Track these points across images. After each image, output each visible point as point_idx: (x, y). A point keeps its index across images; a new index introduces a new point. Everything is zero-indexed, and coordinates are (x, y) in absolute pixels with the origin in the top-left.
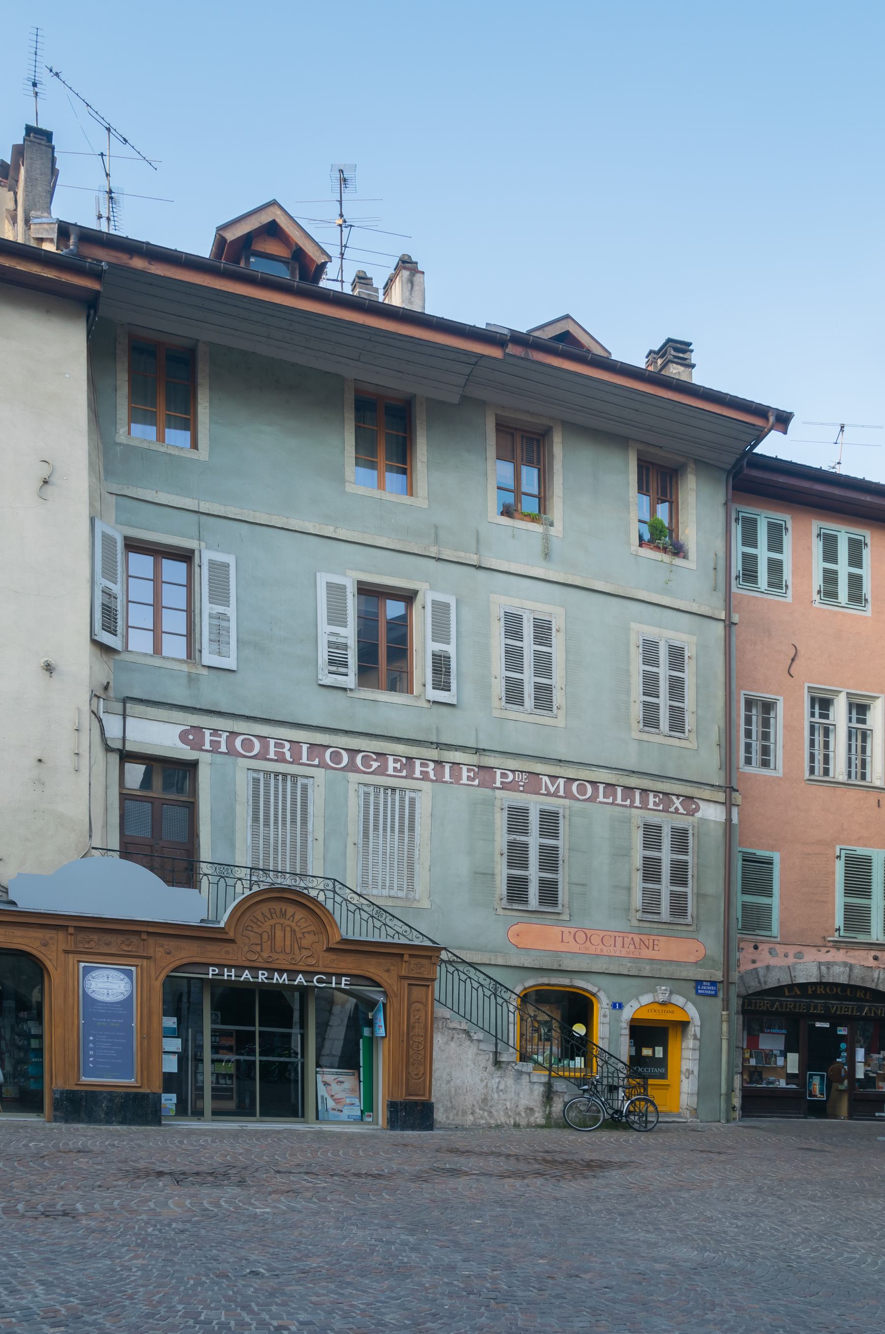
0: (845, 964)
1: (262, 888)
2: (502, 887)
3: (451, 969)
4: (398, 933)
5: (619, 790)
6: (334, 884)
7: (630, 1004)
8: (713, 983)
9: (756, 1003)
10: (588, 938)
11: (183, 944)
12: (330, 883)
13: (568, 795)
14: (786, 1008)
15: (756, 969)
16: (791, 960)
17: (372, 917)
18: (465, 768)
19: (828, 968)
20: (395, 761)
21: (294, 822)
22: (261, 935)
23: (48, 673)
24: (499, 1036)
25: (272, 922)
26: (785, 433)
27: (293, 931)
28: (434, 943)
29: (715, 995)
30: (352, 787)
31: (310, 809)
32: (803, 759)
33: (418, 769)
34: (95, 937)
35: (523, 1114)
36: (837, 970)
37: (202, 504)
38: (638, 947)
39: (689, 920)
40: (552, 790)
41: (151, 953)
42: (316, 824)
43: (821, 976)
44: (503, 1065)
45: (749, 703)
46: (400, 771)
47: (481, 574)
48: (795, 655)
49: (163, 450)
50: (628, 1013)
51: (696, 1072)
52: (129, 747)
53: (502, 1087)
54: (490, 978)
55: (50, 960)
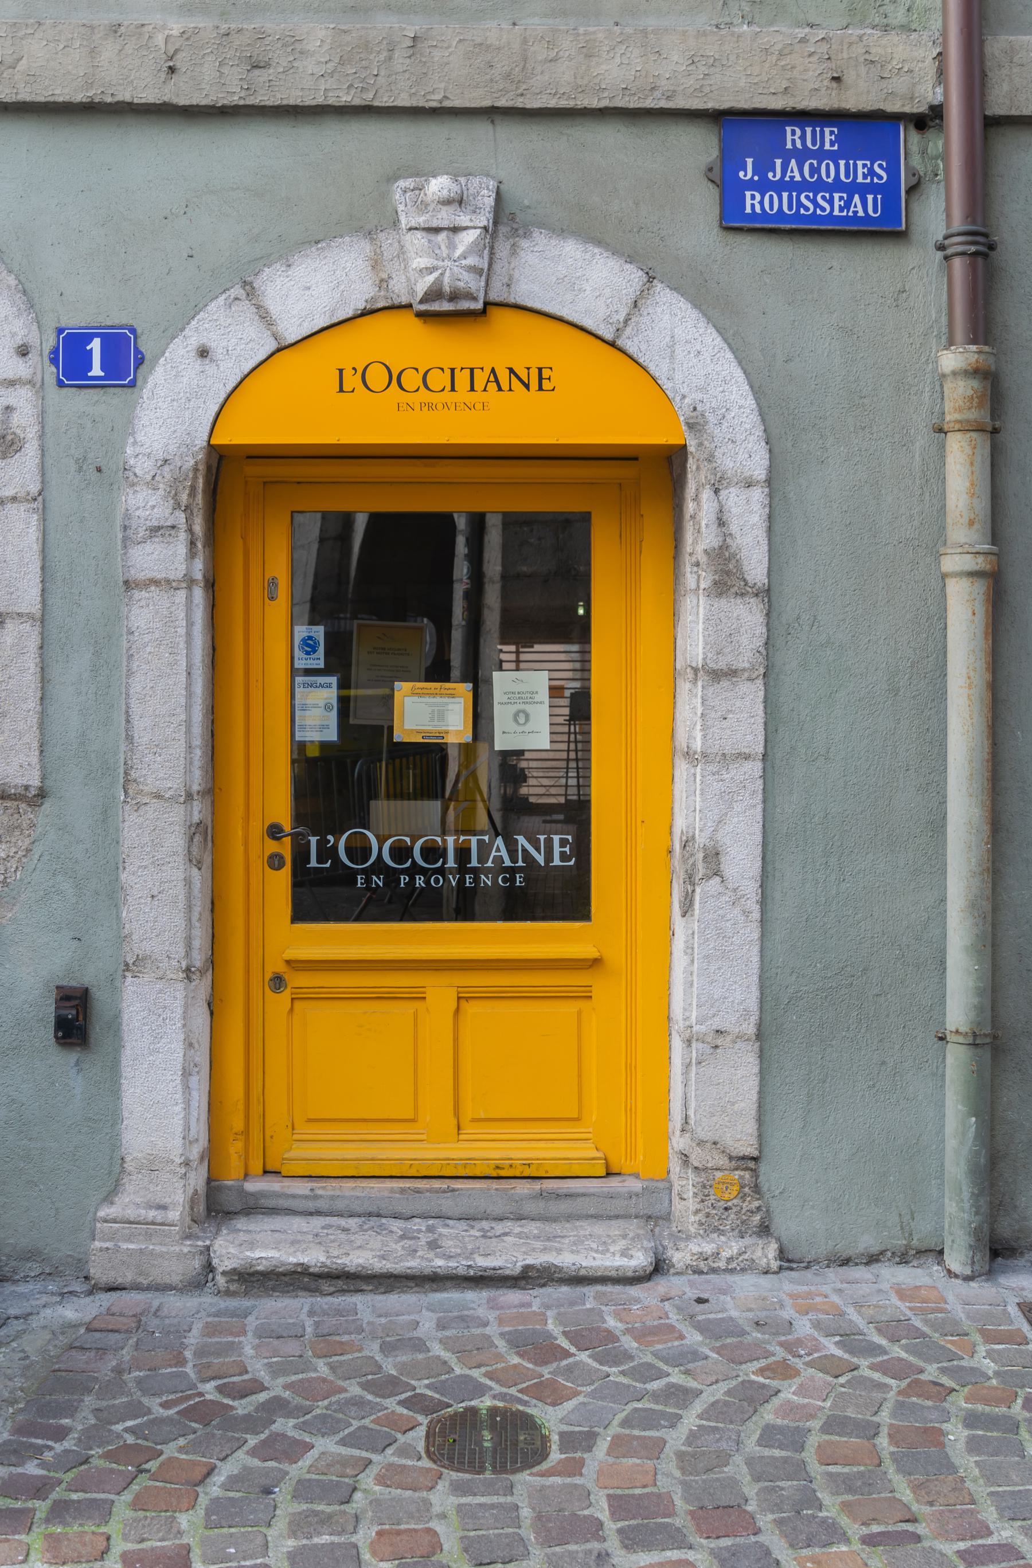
7: (192, 338)
8: (868, 129)
29: (887, 230)
50: (171, 415)
51: (742, 862)
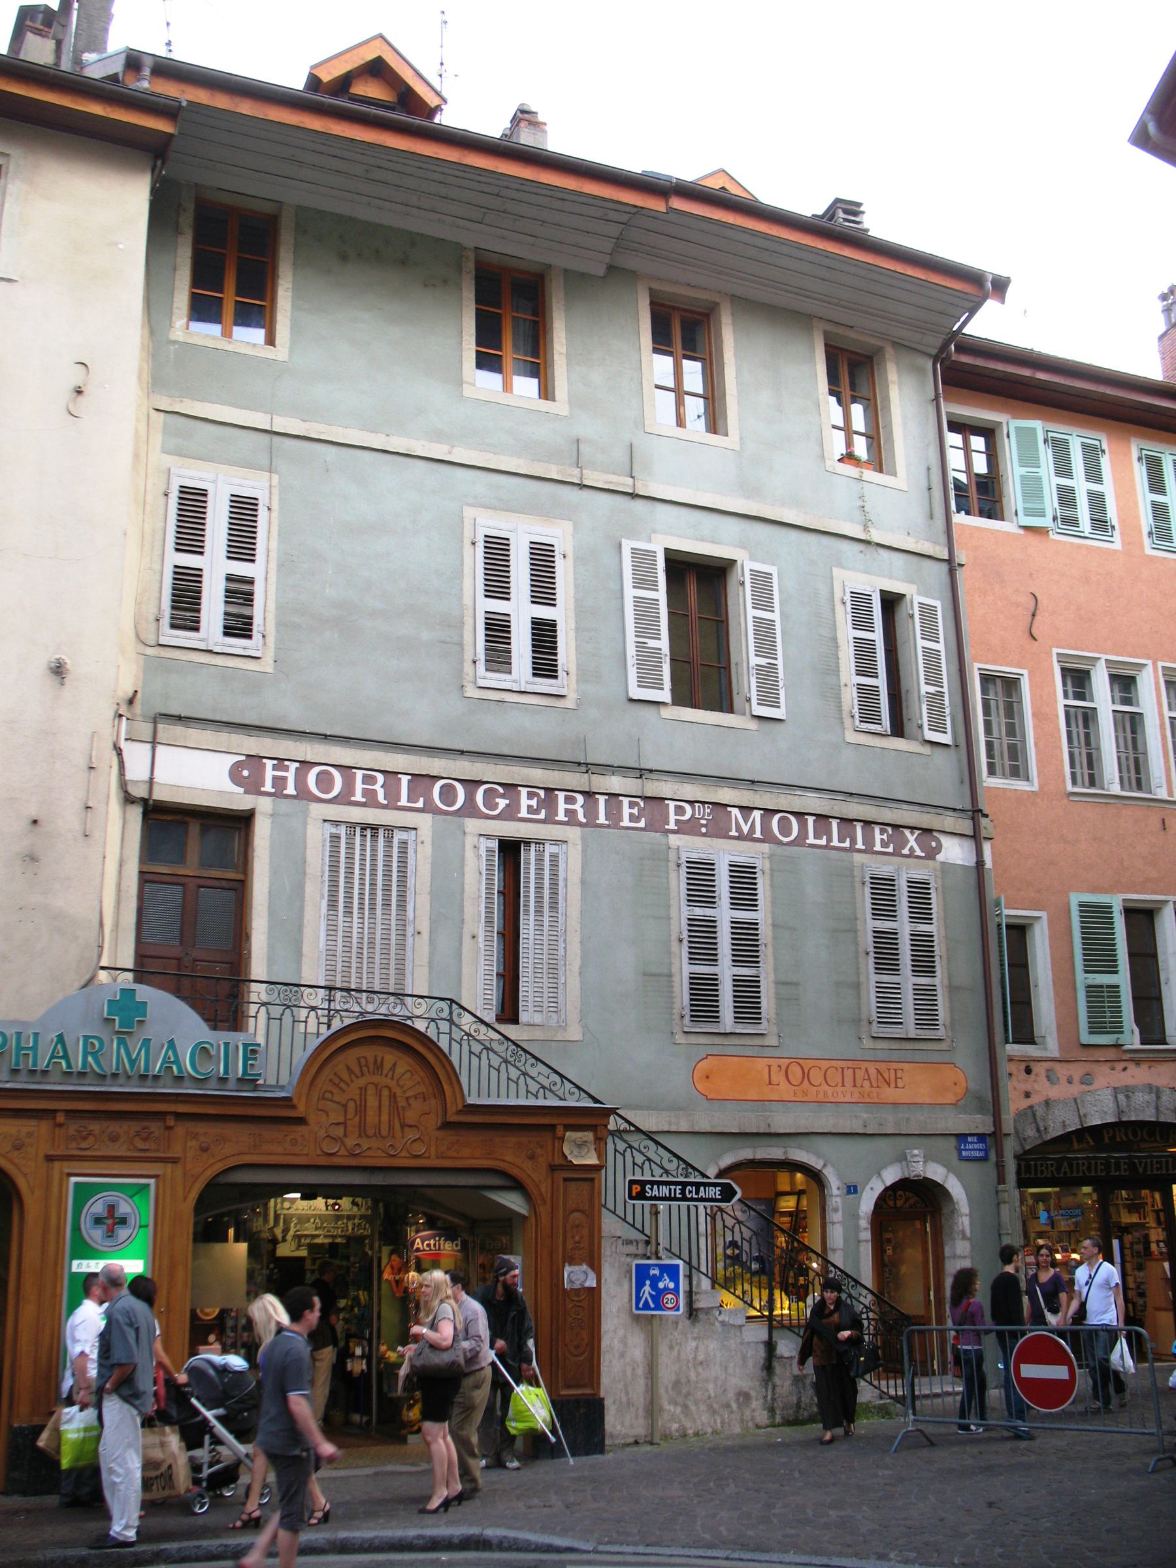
0: (1150, 1088)
1: (347, 1022)
2: (683, 995)
3: (621, 1146)
4: (543, 1087)
5: (834, 824)
6: (450, 1007)
9: (1036, 1165)
10: (806, 1075)
11: (229, 1129)
12: (444, 1005)
13: (768, 837)
14: (1078, 1172)
15: (1031, 1107)
16: (1076, 1089)
17: (506, 1061)
18: (626, 801)
19: (1128, 1097)
20: (531, 796)
21: (387, 905)
22: (345, 1106)
23: (58, 679)
24: (694, 1263)
25: (362, 1082)
26: (1003, 302)
27: (393, 1096)
28: (596, 1101)
29: (984, 1159)
30: (470, 841)
31: (411, 882)
32: (1062, 761)
33: (562, 806)
34: (95, 1126)
35: (734, 1406)
36: (1140, 1098)
37: (277, 420)
38: (874, 1084)
39: (941, 1033)
40: (746, 829)
41: (176, 1151)
42: (420, 907)
43: (1120, 1112)
44: (701, 1316)
45: (987, 679)
46: (537, 812)
47: (639, 505)
48: (1036, 609)
49: (229, 348)
52: (159, 795)
53: (701, 1357)
54: (679, 1158)
55: (25, 1175)
